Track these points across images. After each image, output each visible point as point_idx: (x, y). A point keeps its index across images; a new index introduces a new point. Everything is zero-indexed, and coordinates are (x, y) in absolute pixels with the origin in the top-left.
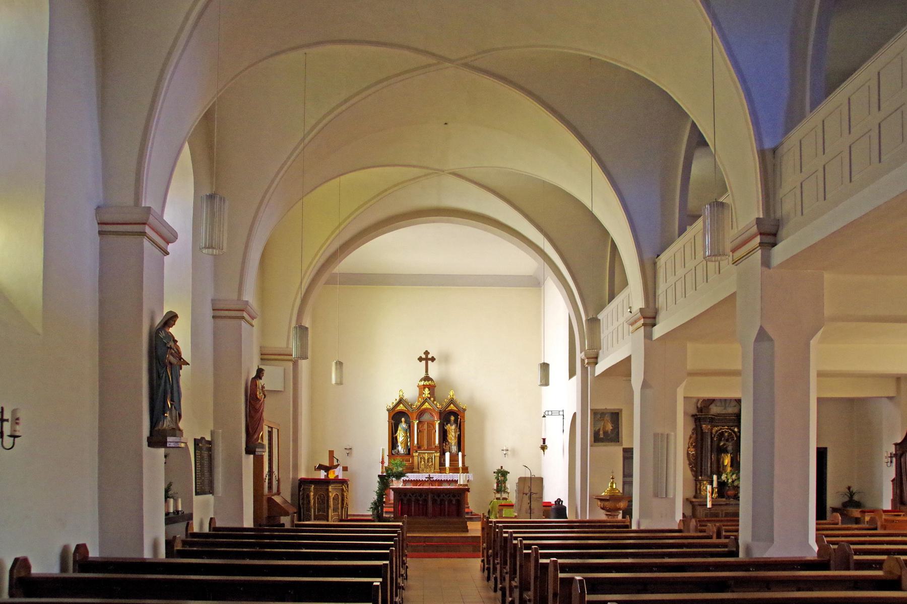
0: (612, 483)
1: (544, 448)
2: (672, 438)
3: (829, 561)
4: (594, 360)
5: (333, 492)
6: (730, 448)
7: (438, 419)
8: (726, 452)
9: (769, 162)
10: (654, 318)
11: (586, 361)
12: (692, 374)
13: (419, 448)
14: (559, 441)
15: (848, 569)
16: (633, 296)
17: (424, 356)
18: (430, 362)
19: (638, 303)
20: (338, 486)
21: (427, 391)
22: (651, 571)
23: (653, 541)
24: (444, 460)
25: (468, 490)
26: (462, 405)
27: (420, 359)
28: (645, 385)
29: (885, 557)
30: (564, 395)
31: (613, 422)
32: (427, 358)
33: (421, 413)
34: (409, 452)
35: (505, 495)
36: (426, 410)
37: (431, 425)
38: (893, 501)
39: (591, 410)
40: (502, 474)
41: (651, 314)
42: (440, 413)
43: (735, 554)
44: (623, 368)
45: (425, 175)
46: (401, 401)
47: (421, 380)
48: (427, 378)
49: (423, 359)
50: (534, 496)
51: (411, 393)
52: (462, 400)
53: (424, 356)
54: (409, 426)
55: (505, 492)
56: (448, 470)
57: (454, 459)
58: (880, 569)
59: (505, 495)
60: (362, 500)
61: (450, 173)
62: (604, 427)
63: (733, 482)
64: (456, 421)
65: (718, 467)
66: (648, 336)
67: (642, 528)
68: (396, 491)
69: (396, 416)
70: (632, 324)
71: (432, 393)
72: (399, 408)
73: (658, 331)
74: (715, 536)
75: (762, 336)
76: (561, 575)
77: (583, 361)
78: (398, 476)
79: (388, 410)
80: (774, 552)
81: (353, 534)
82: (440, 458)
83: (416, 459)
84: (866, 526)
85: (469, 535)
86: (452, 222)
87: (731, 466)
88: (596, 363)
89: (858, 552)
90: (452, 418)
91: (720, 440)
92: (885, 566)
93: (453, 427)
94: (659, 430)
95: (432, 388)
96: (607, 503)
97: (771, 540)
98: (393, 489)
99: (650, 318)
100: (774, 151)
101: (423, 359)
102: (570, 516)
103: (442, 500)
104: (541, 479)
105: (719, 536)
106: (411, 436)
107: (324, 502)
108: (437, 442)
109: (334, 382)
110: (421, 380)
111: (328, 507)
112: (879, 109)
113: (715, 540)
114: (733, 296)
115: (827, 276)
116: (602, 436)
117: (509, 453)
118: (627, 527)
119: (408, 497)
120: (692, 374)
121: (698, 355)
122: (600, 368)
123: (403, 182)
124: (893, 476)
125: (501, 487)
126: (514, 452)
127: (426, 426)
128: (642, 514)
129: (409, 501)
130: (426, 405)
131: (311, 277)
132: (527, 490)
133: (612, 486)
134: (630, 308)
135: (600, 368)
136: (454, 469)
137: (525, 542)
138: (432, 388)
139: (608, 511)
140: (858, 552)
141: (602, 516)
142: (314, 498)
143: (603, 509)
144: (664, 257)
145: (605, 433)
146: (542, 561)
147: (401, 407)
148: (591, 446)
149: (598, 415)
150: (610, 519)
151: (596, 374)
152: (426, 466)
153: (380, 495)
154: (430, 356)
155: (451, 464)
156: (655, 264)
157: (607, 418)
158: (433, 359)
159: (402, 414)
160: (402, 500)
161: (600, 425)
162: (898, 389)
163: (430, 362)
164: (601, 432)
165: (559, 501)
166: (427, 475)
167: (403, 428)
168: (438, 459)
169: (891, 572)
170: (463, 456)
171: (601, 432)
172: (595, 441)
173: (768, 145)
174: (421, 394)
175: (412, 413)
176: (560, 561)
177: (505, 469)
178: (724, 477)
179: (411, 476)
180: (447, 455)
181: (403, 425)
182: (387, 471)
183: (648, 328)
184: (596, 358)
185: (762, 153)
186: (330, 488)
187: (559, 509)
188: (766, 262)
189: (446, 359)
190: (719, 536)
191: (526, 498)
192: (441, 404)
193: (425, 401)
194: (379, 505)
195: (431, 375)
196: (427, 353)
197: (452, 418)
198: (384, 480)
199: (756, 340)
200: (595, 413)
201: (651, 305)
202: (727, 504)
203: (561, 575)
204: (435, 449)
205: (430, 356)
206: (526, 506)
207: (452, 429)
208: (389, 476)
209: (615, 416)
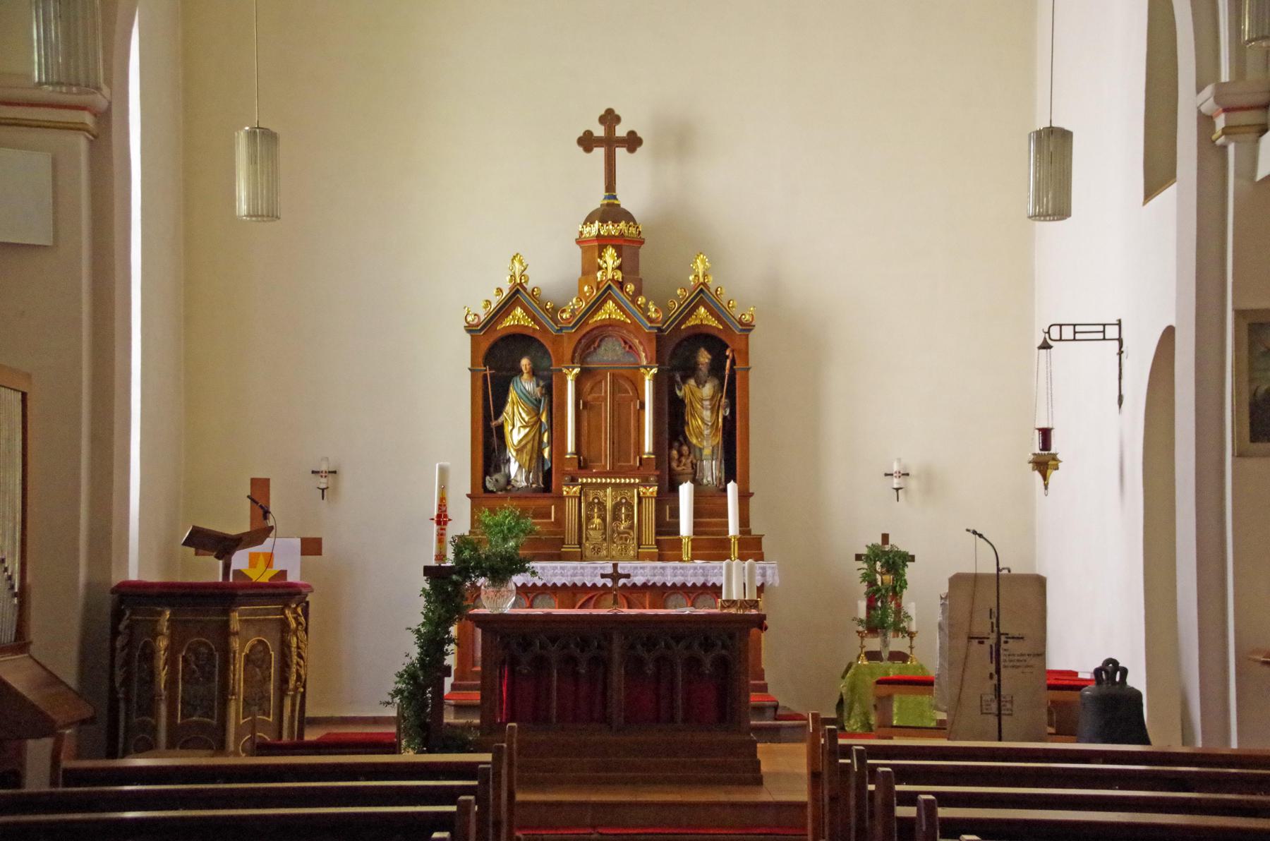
1: (1044, 464)
11: (1220, 122)
13: (584, 465)
18: (621, 152)
21: (610, 258)
24: (675, 513)
26: (740, 310)
27: (587, 142)
32: (609, 139)
33: (590, 339)
34: (546, 482)
35: (898, 643)
36: (610, 324)
37: (628, 382)
39: (1239, 313)
40: (889, 563)
42: (660, 338)
46: (516, 296)
47: (590, 220)
48: (611, 212)
49: (599, 142)
51: (555, 268)
52: (740, 289)
53: (599, 131)
54: (548, 390)
55: (899, 630)
56: (687, 550)
59: (898, 643)
60: (368, 655)
64: (716, 370)
68: (492, 624)
69: (505, 351)
71: (629, 267)
72: (508, 322)
77: (1205, 121)
79: (470, 329)
83: (571, 506)
85: (764, 796)
90: (704, 358)
93: (707, 390)
95: (628, 247)
101: (599, 142)
107: (208, 668)
108: (648, 446)
109: (242, 208)
110: (590, 220)
111: (225, 691)
117: (912, 483)
126: (931, 482)
127: (607, 386)
129: (541, 663)
130: (609, 311)
132: (982, 626)
136: (711, 543)
138: (628, 247)
142: (171, 662)
148: (1239, 454)
153: (433, 644)
158: (633, 142)
159: (520, 342)
163: (621, 152)
167: (526, 396)
168: (650, 508)
172: (1255, 437)
174: (589, 268)
177: (899, 542)
180: (686, 492)
181: (527, 384)
189: (681, 140)
191: (981, 653)
192: (661, 306)
194: (423, 679)
195: (627, 199)
196: (610, 118)
197: (704, 358)
207: (701, 396)
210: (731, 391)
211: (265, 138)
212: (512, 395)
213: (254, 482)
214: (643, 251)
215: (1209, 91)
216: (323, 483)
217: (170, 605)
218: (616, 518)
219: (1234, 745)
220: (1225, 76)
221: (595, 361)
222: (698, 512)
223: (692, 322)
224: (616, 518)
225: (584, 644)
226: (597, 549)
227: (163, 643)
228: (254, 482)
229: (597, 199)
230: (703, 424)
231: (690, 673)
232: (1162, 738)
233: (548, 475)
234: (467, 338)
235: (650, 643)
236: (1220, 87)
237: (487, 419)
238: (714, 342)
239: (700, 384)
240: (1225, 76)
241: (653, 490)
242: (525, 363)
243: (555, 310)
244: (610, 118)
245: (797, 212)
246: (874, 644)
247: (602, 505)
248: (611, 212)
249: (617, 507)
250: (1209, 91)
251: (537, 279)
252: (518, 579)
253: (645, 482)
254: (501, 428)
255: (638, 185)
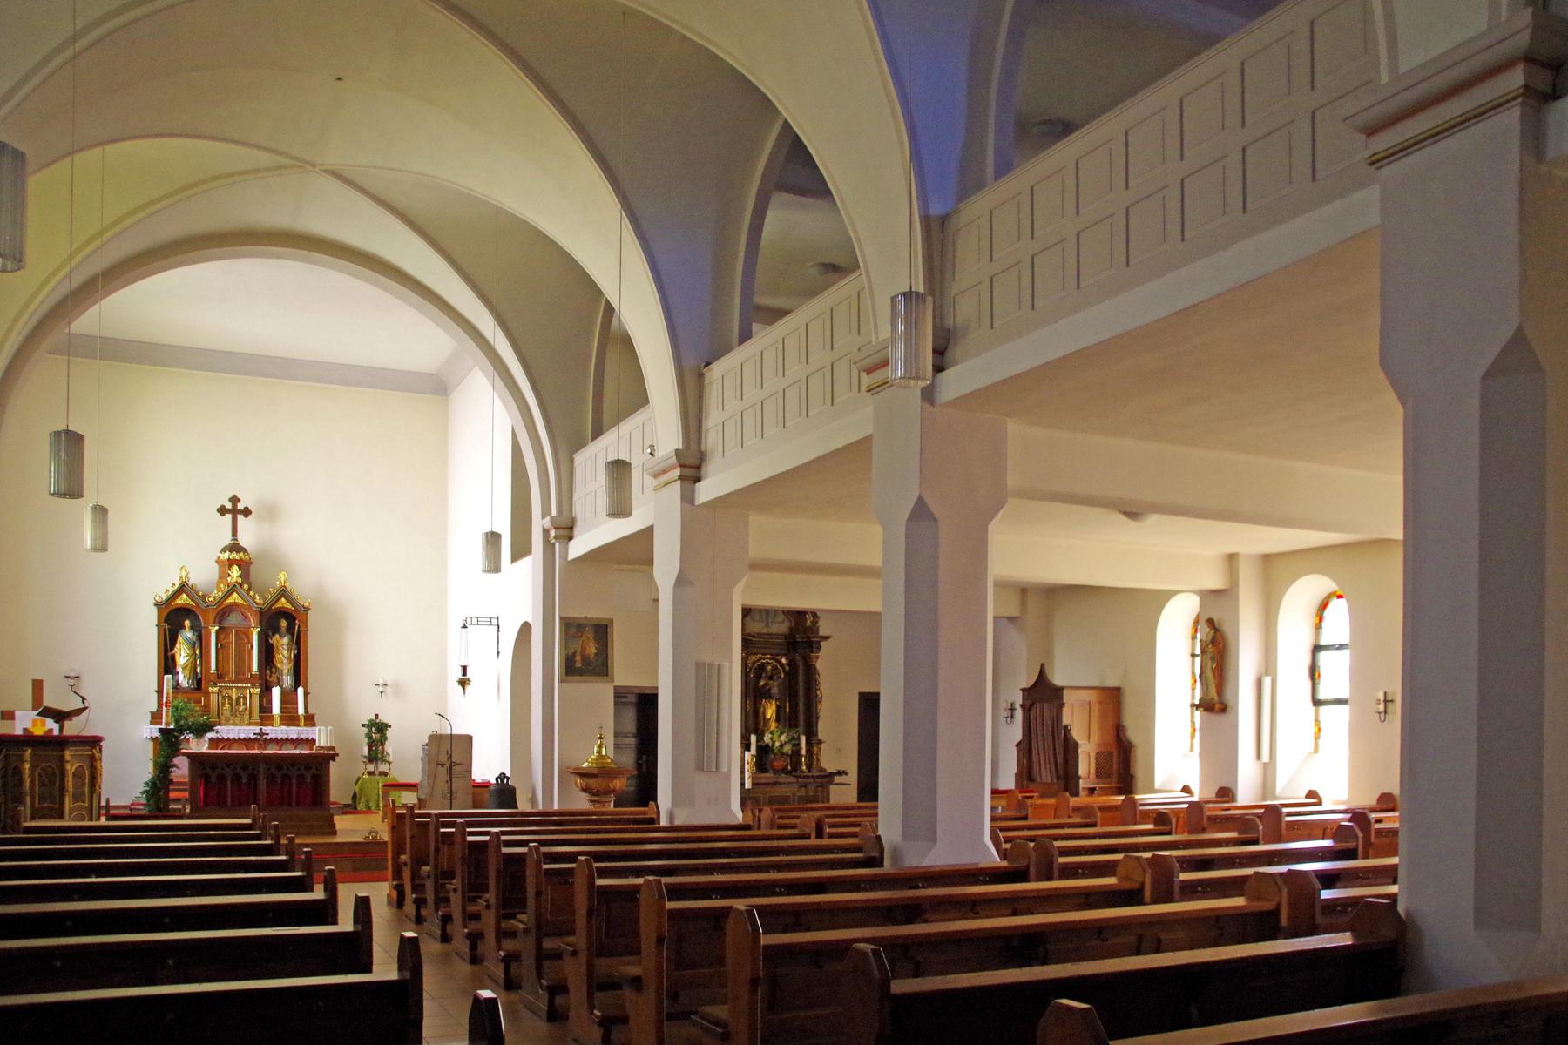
0: (600, 747)
1: (463, 683)
2: (725, 672)
3: (1028, 867)
4: (567, 530)
5: (72, 762)
6: (775, 691)
7: (252, 627)
8: (770, 697)
9: (937, 234)
10: (698, 467)
11: (553, 533)
12: (755, 566)
13: (220, 676)
14: (493, 673)
15: (1049, 878)
16: (656, 428)
17: (229, 506)
18: (240, 517)
19: (669, 439)
20: (85, 751)
21: (235, 571)
22: (858, 889)
23: (696, 845)
24: (270, 702)
25: (333, 757)
26: (303, 601)
27: (222, 511)
28: (681, 581)
29: (1119, 856)
30: (517, 593)
31: (597, 641)
32: (234, 510)
33: (223, 612)
34: (199, 684)
35: (383, 767)
36: (234, 606)
37: (244, 635)
38: (1019, 776)
39: (561, 619)
40: (378, 729)
41: (693, 461)
42: (261, 613)
43: (876, 862)
44: (634, 553)
45: (280, 168)
46: (183, 588)
47: (223, 550)
48: (235, 547)
49: (228, 511)
50: (456, 768)
51: (204, 573)
52: (303, 591)
53: (229, 506)
54: (200, 637)
55: (383, 761)
56: (277, 720)
57: (288, 699)
58: (1113, 874)
59: (383, 767)
60: (126, 775)
61: (327, 171)
62: (583, 649)
63: (782, 746)
64: (290, 630)
65: (756, 722)
66: (688, 498)
67: (678, 822)
68: (194, 758)
69: (175, 617)
70: (656, 476)
71: (245, 575)
72: (179, 601)
73: (706, 491)
74: (814, 835)
75: (921, 512)
76: (669, 905)
77: (546, 532)
78: (200, 730)
79: (157, 604)
80: (940, 857)
81: (114, 847)
82: (261, 697)
83: (213, 698)
84: (765, 831)
85: (339, 839)
86: (244, 256)
87: (777, 720)
88: (571, 538)
89: (1066, 852)
90: (284, 624)
91: (759, 677)
92: (1119, 869)
93: (286, 640)
94: (706, 658)
95: (244, 566)
96: (592, 782)
97: (933, 839)
98: (189, 756)
99: (691, 467)
100: (944, 220)
101: (228, 511)
102: (523, 805)
103: (221, 778)
104: (469, 738)
105: (820, 835)
106: (204, 655)
107: (53, 782)
108: (255, 667)
109: (88, 544)
110: (223, 550)
111: (63, 789)
112: (1127, 187)
113: (814, 842)
114: (868, 440)
115: (1013, 427)
116: (579, 665)
117: (388, 690)
118: (652, 821)
119: (218, 771)
120: (755, 566)
121: (766, 535)
122: (579, 547)
123: (231, 175)
124: (1018, 736)
125: (376, 751)
126: (398, 689)
127: (233, 637)
128: (676, 800)
129: (221, 778)
130: (235, 598)
131: (25, 333)
132: (443, 758)
133: (599, 752)
134: (652, 446)
135: (579, 547)
136: (289, 718)
137: (544, 849)
138: (244, 566)
139: (593, 794)
140: (1066, 852)
141: (582, 803)
142: (32, 775)
143: (584, 790)
144: (718, 369)
145: (585, 659)
146: (600, 882)
147: (184, 599)
148: (562, 681)
149: (572, 628)
150: (598, 808)
151: (571, 556)
152: (234, 713)
153: (163, 769)
154: (240, 506)
155: (283, 709)
156: (701, 376)
157: (589, 633)
158: (247, 512)
159: (185, 612)
160: (207, 778)
161: (576, 646)
162: (1023, 604)
163: (240, 517)
164: (578, 658)
165: (502, 776)
166: (257, 729)
167: (188, 641)
168: (256, 699)
169: (1127, 878)
170: (306, 694)
171: (578, 658)
172: (568, 673)
173: (936, 210)
174: (223, 576)
175: (206, 611)
176: (665, 880)
177: (384, 719)
178: (767, 738)
179: (224, 731)
180: (276, 692)
181: (188, 634)
182: (177, 721)
183: (688, 485)
184: (571, 528)
185: (926, 221)
186: (68, 754)
187: (504, 792)
188: (928, 395)
189: (272, 513)
190: (820, 835)
191: (442, 772)
192: (262, 597)
193: (233, 589)
194: (161, 784)
195: (242, 541)
196: (235, 500)
197: (284, 624)
198: (168, 743)
199: (910, 519)
200: (567, 623)
201: (693, 447)
202: (775, 783)
203: (669, 905)
204: (252, 680)
205: (240, 506)
206: (442, 786)
207: (282, 643)
208: (181, 730)
209: (602, 631)
210: (298, 641)
211: (101, 512)
212: (180, 639)
213: (35, 682)
214: (252, 568)
215: (548, 519)
216: (72, 682)
217: (33, 747)
218: (238, 704)
219: (556, 807)
220: (554, 513)
221: (226, 624)
222: (283, 702)
223: (278, 605)
224: (238, 704)
225: (279, 768)
226: (227, 720)
227: (27, 766)
228: (35, 682)
229: (227, 540)
230: (283, 657)
231: (298, 781)
232: (523, 805)
233: (199, 682)
234: (155, 610)
235: (279, 768)
236: (553, 519)
237: (166, 651)
238: (289, 616)
239: (282, 637)
240: (554, 513)
241: (258, 690)
242: (187, 623)
243: (204, 597)
244: (235, 500)
245: (318, 552)
246: (371, 768)
247: (230, 698)
248: (235, 547)
249: (238, 699)
250: (548, 519)
251: (194, 580)
252: (210, 735)
253: (254, 686)
254: (173, 657)
255: (249, 534)
